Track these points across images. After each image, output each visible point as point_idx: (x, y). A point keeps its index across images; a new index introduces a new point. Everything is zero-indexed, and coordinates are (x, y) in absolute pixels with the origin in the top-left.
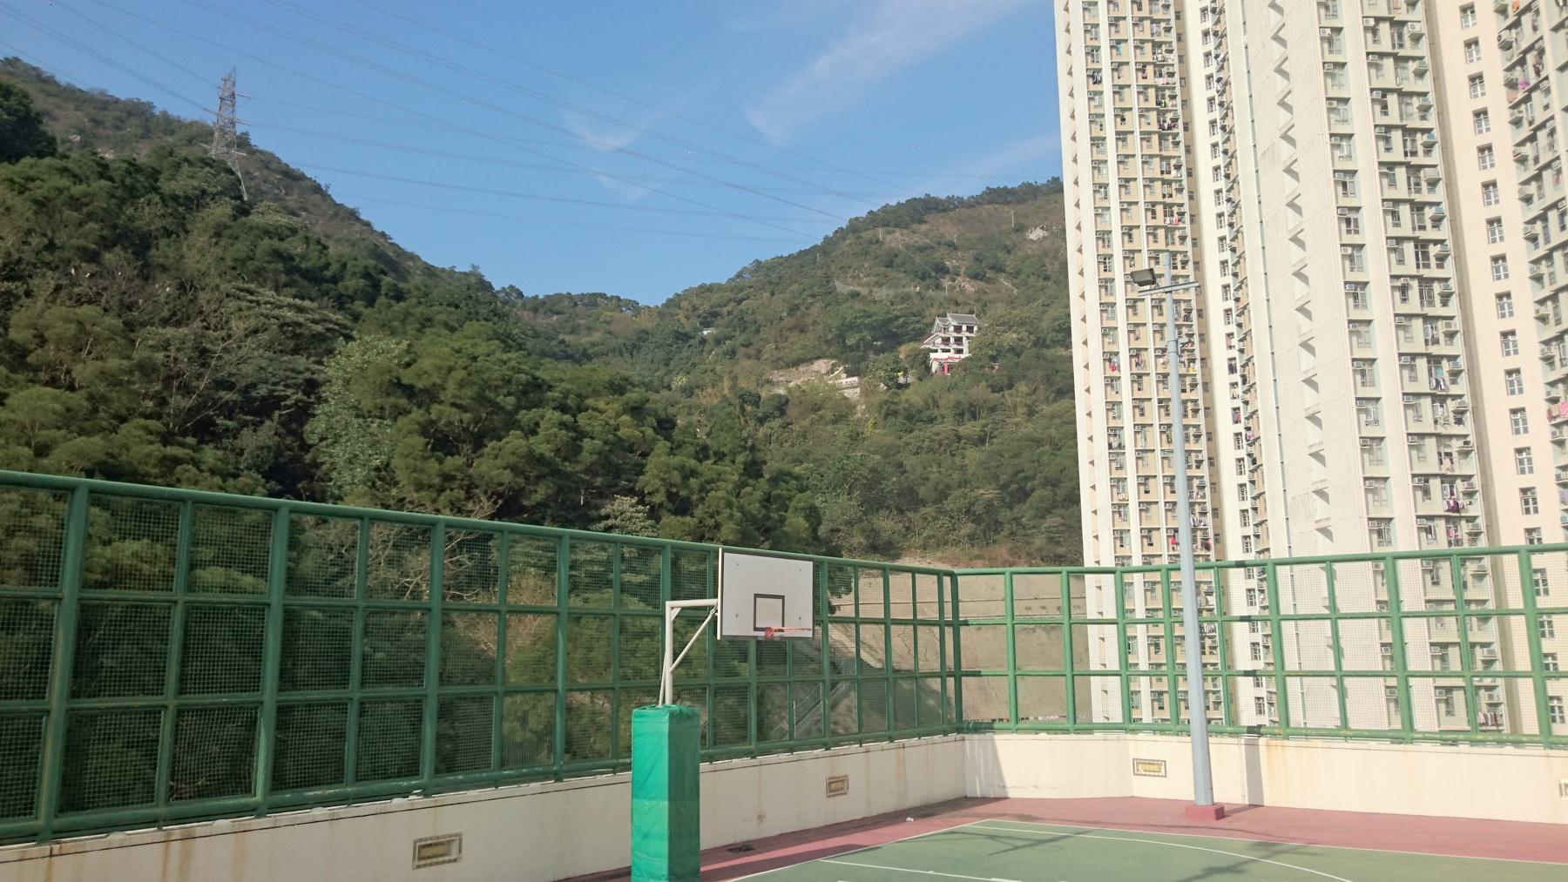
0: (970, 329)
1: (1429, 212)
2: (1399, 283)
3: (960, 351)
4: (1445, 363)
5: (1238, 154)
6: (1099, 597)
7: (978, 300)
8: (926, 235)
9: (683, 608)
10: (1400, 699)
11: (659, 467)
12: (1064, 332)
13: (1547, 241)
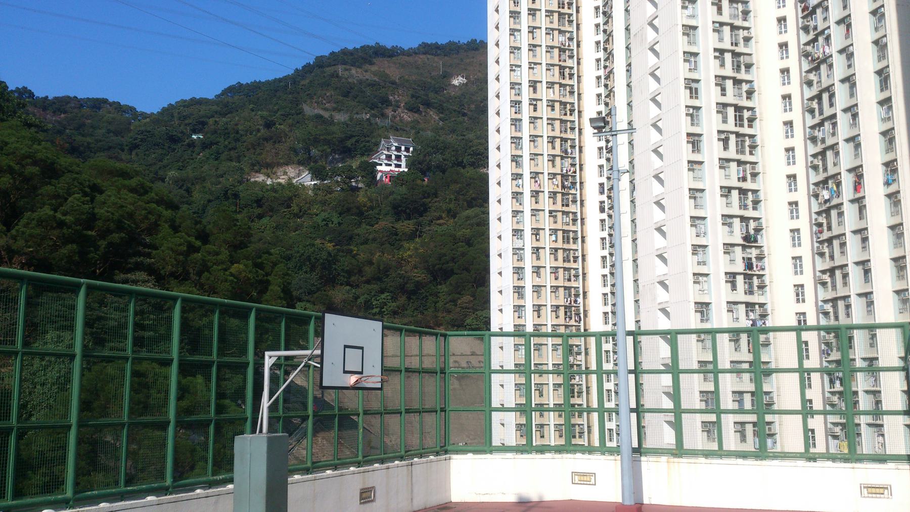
0: (407, 150)
1: (745, 87)
2: (723, 136)
3: (399, 166)
4: (750, 193)
5: (614, 33)
6: (503, 354)
7: (412, 128)
8: (375, 74)
9: (279, 358)
10: (712, 429)
11: (167, 246)
12: (481, 157)
13: (821, 113)
